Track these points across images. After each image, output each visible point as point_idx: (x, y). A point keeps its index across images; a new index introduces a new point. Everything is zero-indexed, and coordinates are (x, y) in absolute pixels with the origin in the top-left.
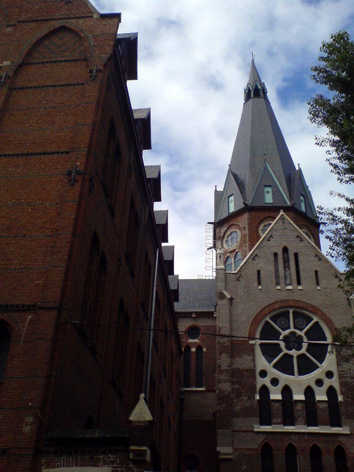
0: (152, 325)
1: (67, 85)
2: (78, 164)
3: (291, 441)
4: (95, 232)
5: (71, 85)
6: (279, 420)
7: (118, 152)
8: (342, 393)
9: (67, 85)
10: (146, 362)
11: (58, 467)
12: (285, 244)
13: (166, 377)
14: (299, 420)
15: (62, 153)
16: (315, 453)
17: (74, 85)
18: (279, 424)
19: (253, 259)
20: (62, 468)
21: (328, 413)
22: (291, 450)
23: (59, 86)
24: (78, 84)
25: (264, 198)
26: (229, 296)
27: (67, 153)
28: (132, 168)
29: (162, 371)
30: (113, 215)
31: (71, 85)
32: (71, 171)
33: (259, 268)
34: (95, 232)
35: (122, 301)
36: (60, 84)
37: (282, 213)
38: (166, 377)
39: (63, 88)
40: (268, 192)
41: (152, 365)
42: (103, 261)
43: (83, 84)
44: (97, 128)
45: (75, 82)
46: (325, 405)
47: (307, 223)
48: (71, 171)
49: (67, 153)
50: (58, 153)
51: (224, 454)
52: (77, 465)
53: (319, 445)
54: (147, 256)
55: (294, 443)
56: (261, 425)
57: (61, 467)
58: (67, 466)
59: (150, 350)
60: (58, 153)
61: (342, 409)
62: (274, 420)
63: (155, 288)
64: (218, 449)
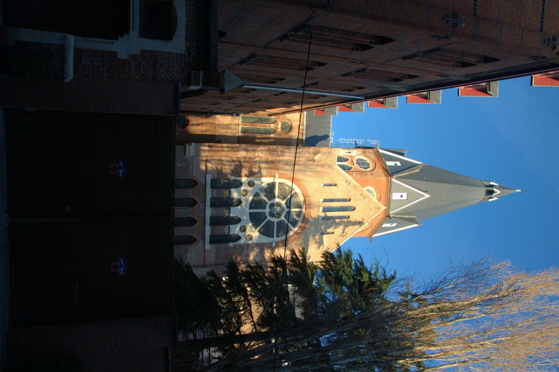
0: (308, 92)
1: (543, 14)
2: (463, 25)
3: (199, 203)
4: (394, 40)
5: (542, 18)
6: (215, 195)
7: (465, 65)
8: (235, 246)
9: (543, 14)
10: (342, 92)
11: (186, 4)
12: (358, 208)
13: (253, 102)
14: (215, 211)
15: (475, 10)
16: (193, 222)
17: (542, 22)
18: (212, 194)
19: (346, 181)
20: (185, 8)
21: (220, 234)
22: (194, 203)
23: (544, 5)
24: (542, 26)
25: (397, 192)
26: (316, 158)
27: (475, 14)
28: (445, 78)
29: (257, 99)
30: (405, 58)
31: (542, 18)
32: (456, 18)
33: (338, 185)
34: (394, 40)
35: (324, 64)
36: (546, 6)
37: (385, 208)
38: (253, 102)
39: (541, 9)
40: (401, 196)
41: (264, 90)
42: (365, 48)
43: (541, 31)
44: (330, 44)
45: (545, 23)
46: (226, 233)
47: (373, 227)
48: (456, 18)
49: (475, 14)
50: (475, 5)
51: (189, 149)
52: (187, 21)
53: (196, 225)
54: (360, 88)
55: (197, 205)
56: (211, 180)
57: (186, 7)
58: (186, 12)
59: (277, 89)
60: (475, 5)
61: (223, 245)
62: (214, 191)
63: (330, 94)
64: (193, 144)
